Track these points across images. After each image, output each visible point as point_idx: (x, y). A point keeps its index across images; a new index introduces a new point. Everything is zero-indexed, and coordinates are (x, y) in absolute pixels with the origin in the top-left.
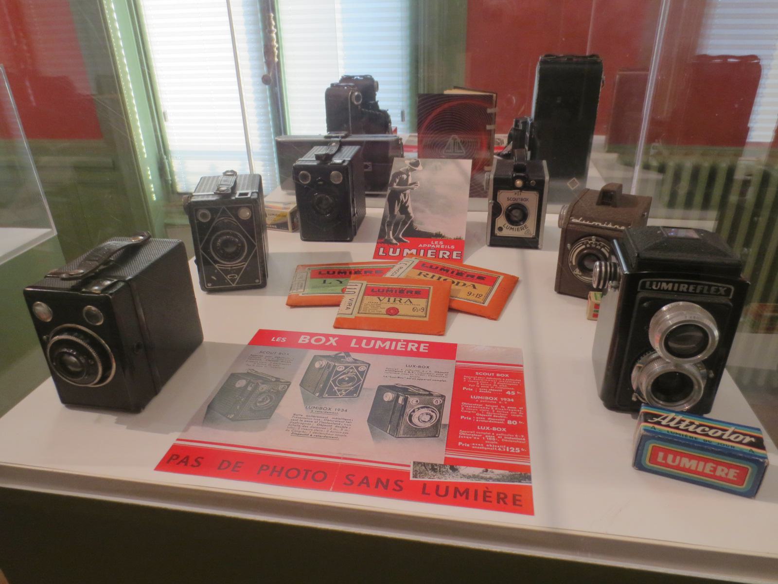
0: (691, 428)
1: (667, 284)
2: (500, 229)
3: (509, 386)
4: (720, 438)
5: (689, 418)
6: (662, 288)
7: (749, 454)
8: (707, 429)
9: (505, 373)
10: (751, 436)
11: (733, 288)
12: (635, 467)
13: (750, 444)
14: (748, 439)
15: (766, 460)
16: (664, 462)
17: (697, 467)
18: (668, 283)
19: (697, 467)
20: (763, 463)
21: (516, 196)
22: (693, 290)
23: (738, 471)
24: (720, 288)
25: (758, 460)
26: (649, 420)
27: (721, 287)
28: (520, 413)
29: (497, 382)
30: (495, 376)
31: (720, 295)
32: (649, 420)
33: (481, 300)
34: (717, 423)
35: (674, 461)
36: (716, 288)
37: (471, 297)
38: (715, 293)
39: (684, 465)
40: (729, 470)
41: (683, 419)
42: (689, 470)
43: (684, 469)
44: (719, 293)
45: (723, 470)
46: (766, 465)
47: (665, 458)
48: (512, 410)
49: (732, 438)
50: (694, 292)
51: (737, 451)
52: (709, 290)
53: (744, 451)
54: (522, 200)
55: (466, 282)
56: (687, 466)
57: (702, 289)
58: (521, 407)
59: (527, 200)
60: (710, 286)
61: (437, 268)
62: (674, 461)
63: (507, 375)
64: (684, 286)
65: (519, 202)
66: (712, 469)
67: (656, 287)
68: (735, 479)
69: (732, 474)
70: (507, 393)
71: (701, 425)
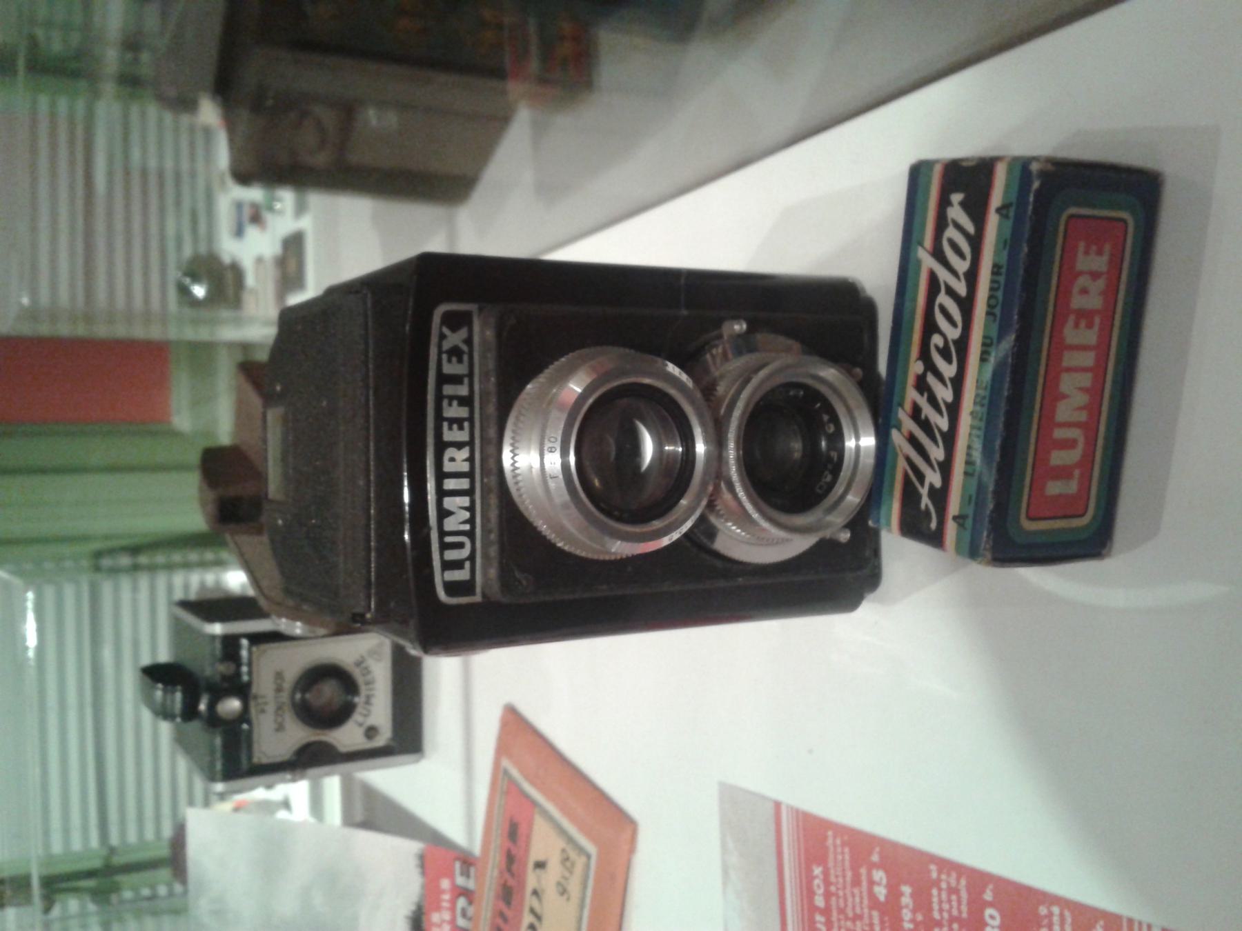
0: (944, 394)
1: (450, 513)
2: (371, 732)
3: (856, 882)
4: (966, 305)
5: (904, 389)
6: (467, 527)
7: (1018, 220)
8: (937, 340)
9: (810, 878)
10: (944, 203)
11: (442, 309)
12: (1104, 552)
13: (976, 209)
14: (956, 213)
15: (1035, 167)
16: (1077, 473)
17: (1084, 370)
18: (443, 514)
19: (1084, 370)
20: (1043, 174)
21: (271, 708)
22: (461, 428)
23: (1082, 246)
24: (446, 345)
25: (1038, 193)
26: (933, 525)
27: (440, 346)
28: (953, 883)
29: (847, 919)
30: (826, 911)
31: (469, 341)
32: (933, 525)
33: (580, 862)
34: (910, 284)
35: (1069, 444)
36: (444, 357)
37: (574, 887)
38: (466, 358)
39: (1080, 409)
40: (1081, 273)
41: (908, 406)
42: (1095, 392)
43: (1093, 409)
44: (465, 348)
45: (1084, 291)
46: (1050, 167)
47: (1063, 473)
48: (946, 906)
49: (962, 266)
50: (466, 424)
51: (1012, 257)
52: (456, 380)
53: (1008, 233)
54: (279, 690)
55: (529, 890)
56: (1082, 399)
57: (455, 403)
58: (929, 871)
59: (279, 676)
60: (443, 379)
61: (501, 915)
62: (1069, 444)
63: (818, 871)
64: (452, 460)
65: (285, 697)
66: (1083, 323)
67: (460, 546)
68: (1107, 248)
69: (1091, 261)
70: (882, 898)
71: (925, 356)
